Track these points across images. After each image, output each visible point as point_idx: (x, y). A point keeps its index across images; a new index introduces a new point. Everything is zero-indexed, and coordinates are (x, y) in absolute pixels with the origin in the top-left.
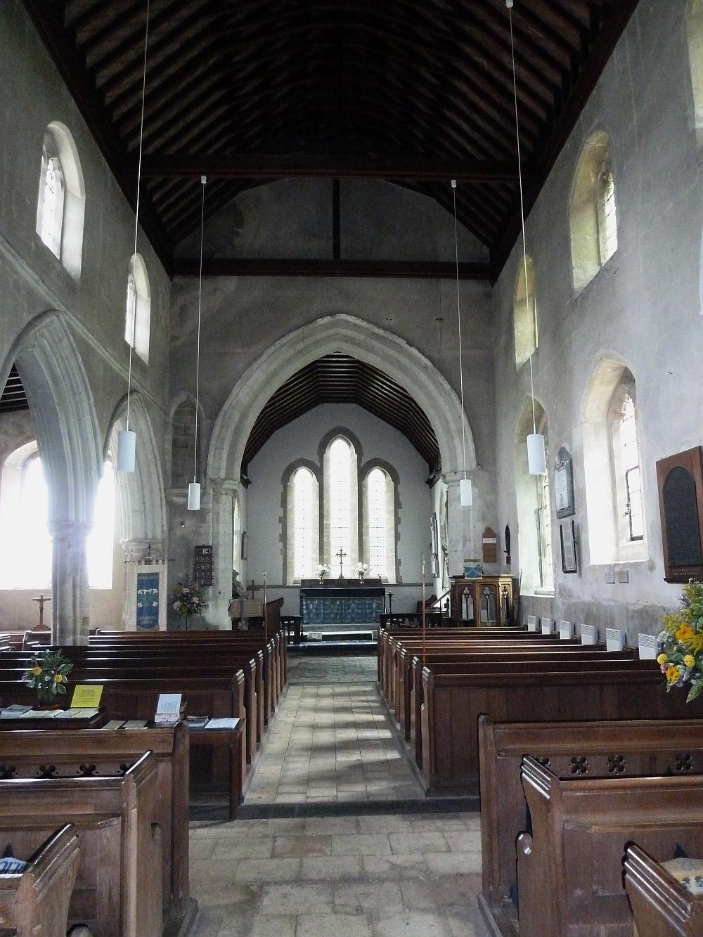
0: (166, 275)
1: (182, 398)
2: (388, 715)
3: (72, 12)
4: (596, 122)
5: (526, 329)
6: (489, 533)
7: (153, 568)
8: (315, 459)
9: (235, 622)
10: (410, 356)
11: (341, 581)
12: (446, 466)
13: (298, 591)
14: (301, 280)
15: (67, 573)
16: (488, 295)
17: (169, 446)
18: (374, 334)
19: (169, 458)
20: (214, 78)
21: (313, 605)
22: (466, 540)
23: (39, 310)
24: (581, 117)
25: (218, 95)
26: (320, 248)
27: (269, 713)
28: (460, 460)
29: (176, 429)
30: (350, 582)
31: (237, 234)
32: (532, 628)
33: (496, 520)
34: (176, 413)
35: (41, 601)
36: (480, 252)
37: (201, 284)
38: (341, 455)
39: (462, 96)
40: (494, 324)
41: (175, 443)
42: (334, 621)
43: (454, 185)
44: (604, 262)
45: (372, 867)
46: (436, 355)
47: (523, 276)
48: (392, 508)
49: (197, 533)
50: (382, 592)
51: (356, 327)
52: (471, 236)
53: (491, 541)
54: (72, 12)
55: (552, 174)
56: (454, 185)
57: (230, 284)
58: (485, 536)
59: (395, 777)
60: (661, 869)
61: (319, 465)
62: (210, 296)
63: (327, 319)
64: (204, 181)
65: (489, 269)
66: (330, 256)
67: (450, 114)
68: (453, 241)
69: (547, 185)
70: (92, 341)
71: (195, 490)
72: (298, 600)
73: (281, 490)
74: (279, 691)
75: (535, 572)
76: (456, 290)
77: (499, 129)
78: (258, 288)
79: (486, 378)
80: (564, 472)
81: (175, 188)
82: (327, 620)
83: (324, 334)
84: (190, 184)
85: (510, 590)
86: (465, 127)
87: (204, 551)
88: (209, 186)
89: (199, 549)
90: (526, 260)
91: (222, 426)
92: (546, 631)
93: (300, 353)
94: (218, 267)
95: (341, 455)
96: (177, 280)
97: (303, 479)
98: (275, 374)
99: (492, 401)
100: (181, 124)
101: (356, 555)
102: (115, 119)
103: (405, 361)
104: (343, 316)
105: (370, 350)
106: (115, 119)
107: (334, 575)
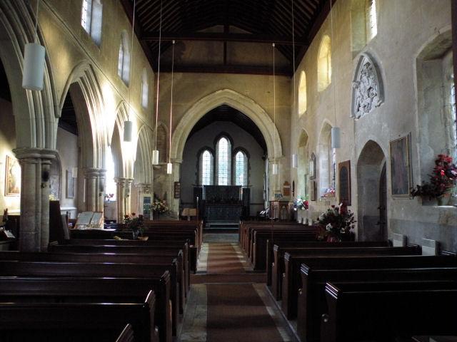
2: (243, 252)
6: (286, 183)
8: (212, 147)
11: (451, 256)
12: (270, 155)
20: (179, 17)
22: (277, 186)
27: (178, 315)
28: (275, 152)
31: (182, 54)
32: (300, 222)
38: (224, 145)
39: (277, 10)
40: (289, 92)
46: (266, 108)
48: (246, 169)
57: (180, 75)
58: (285, 185)
62: (174, 78)
63: (220, 91)
66: (228, 43)
68: (273, 58)
73: (197, 160)
74: (187, 287)
76: (274, 79)
77: (230, 249)
78: (190, 78)
80: (312, 162)
83: (219, 97)
93: (208, 105)
95: (224, 145)
96: (152, 338)
98: (197, 114)
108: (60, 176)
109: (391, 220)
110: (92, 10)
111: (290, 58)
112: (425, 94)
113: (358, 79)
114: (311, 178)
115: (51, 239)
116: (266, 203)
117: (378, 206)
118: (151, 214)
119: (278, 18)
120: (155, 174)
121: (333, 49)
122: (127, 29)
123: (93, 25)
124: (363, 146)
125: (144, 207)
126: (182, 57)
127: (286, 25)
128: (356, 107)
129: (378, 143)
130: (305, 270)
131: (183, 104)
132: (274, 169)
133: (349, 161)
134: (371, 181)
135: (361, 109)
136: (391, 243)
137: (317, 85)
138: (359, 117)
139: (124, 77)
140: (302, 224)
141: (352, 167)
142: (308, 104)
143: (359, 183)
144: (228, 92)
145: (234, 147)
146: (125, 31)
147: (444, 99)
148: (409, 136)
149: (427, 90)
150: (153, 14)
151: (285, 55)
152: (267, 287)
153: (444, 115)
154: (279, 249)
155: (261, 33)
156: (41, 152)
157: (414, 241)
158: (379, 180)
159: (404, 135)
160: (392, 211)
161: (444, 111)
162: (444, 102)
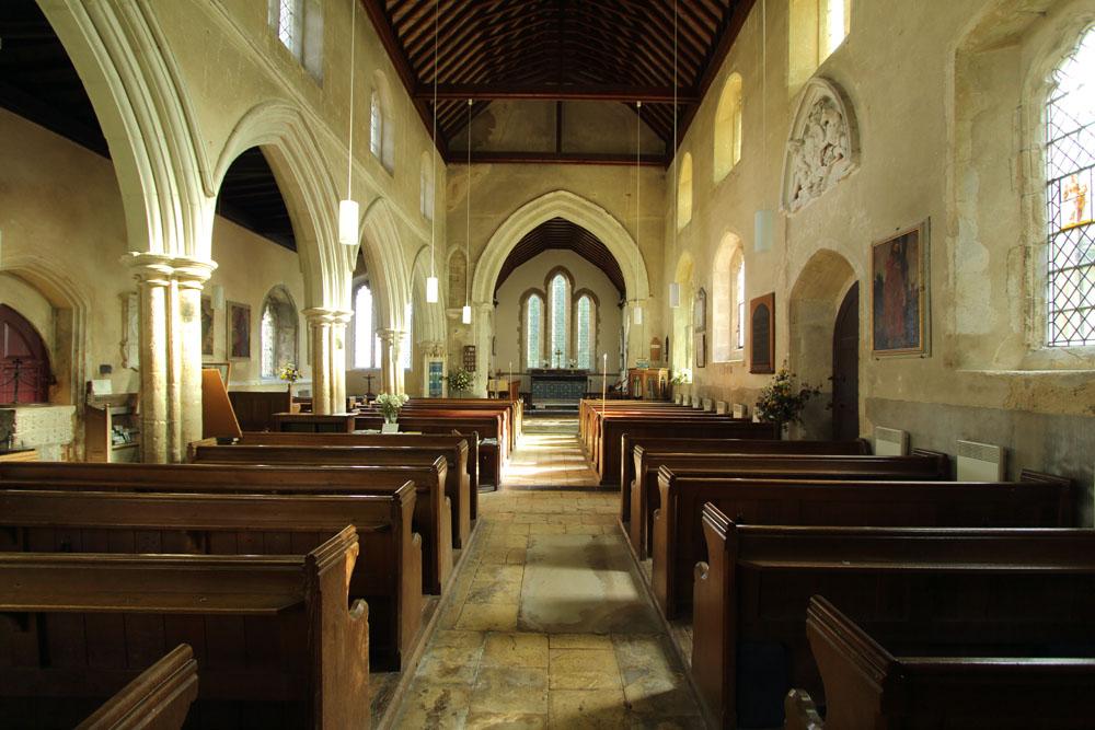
0: (443, 163)
1: (455, 248)
3: (389, 5)
4: (734, 66)
5: (685, 202)
6: (656, 341)
7: (438, 360)
9: (490, 393)
10: (606, 219)
11: (558, 370)
12: (629, 295)
13: (529, 377)
14: (533, 167)
15: (373, 365)
16: (664, 177)
17: (447, 281)
18: (583, 205)
19: (447, 288)
21: (539, 385)
23: (374, 198)
24: (726, 61)
25: (478, 36)
26: (545, 144)
29: (451, 268)
30: (564, 371)
31: (490, 133)
32: (677, 402)
33: (661, 335)
34: (452, 258)
35: (369, 378)
36: (658, 145)
37: (469, 169)
38: (559, 285)
40: (663, 193)
41: (451, 279)
42: (552, 397)
43: (639, 105)
44: (735, 163)
45: (566, 509)
47: (685, 166)
49: (465, 337)
50: (585, 379)
51: (571, 200)
52: (653, 134)
53: (657, 346)
54: (389, 5)
55: (706, 98)
56: (639, 105)
57: (486, 169)
59: (583, 477)
60: (853, 635)
61: (544, 291)
62: (476, 176)
63: (552, 194)
64: (470, 103)
65: (661, 160)
67: (641, 47)
68: (639, 137)
69: (703, 104)
70: (402, 215)
71: (467, 312)
72: (529, 383)
75: (683, 368)
76: (637, 172)
78: (503, 172)
79: (658, 234)
81: (454, 107)
82: (545, 397)
84: (462, 105)
85: (666, 378)
86: (651, 58)
87: (471, 349)
88: (473, 106)
89: (467, 348)
90: (688, 156)
91: (482, 267)
92: (685, 403)
94: (481, 157)
95: (559, 285)
97: (534, 302)
99: (662, 253)
100: (453, 58)
101: (568, 354)
102: (411, 57)
103: (605, 225)
104: (563, 192)
105: (579, 215)
106: (411, 57)
107: (554, 366)
108: (297, 328)
109: (867, 400)
110: (304, 16)
111: (665, 125)
112: (973, 127)
113: (799, 135)
114: (697, 331)
115: (206, 435)
116: (624, 374)
117: (831, 374)
118: (444, 383)
119: (647, 59)
120: (449, 327)
121: (747, 96)
122: (384, 71)
123: (308, 48)
124: (803, 263)
125: (204, 366)
126: (490, 138)
127: (663, 75)
128: (792, 191)
129: (843, 253)
130: (715, 521)
131: (493, 216)
132: (637, 317)
133: (774, 294)
134: (818, 328)
135: (804, 193)
136: (868, 447)
137: (712, 171)
138: (798, 209)
139: (386, 159)
140: (681, 406)
141: (778, 306)
142: (694, 209)
143: (93, 563)
144: (565, 197)
145: (576, 290)
146: (380, 73)
147: (1022, 134)
148: (927, 224)
149: (976, 120)
150: (449, 68)
151: (656, 131)
152: (622, 524)
153: (1021, 171)
154: (672, 481)
155: (614, 78)
156: (175, 263)
157: (936, 441)
158: (833, 326)
159: (905, 228)
160: (873, 382)
161: (1021, 164)
162: (1022, 142)
